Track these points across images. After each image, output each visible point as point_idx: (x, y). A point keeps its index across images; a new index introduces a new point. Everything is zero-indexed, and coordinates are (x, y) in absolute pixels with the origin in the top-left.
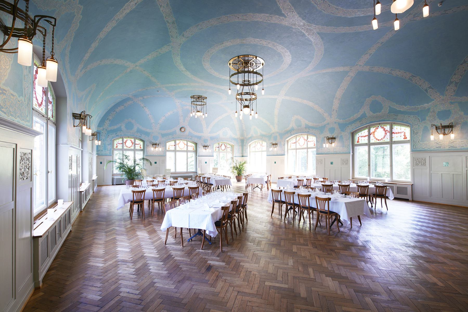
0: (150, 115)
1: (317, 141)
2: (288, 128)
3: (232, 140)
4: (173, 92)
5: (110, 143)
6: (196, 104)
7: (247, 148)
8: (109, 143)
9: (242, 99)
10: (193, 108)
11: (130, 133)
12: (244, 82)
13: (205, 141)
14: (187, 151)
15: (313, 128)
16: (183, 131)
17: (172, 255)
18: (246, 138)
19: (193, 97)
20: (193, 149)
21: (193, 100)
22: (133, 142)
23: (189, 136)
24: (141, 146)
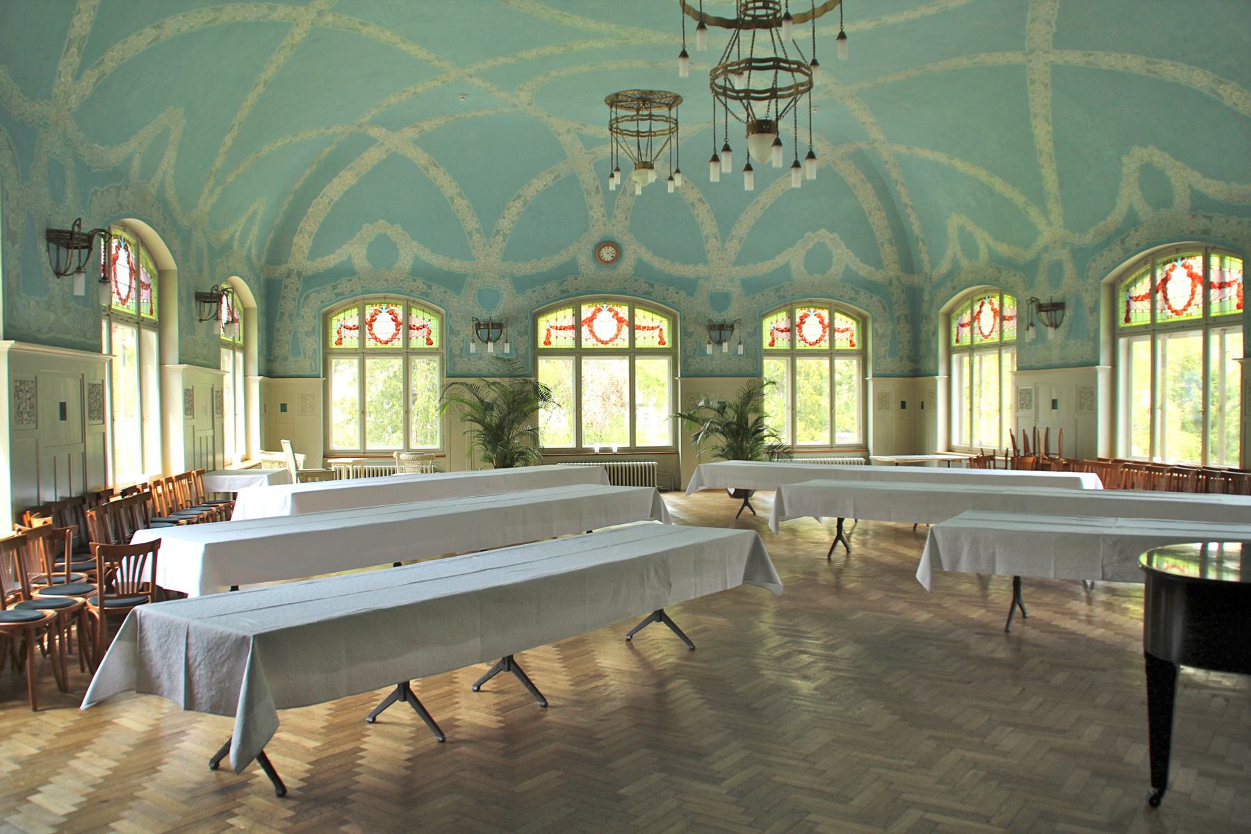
0: (458, 201)
2: (1109, 219)
3: (857, 293)
4: (521, 90)
5: (314, 328)
7: (935, 333)
8: (310, 329)
9: (730, 90)
11: (387, 280)
13: (721, 300)
14: (632, 353)
17: (251, 785)
18: (931, 278)
20: (662, 342)
22: (400, 318)
24: (852, 335)
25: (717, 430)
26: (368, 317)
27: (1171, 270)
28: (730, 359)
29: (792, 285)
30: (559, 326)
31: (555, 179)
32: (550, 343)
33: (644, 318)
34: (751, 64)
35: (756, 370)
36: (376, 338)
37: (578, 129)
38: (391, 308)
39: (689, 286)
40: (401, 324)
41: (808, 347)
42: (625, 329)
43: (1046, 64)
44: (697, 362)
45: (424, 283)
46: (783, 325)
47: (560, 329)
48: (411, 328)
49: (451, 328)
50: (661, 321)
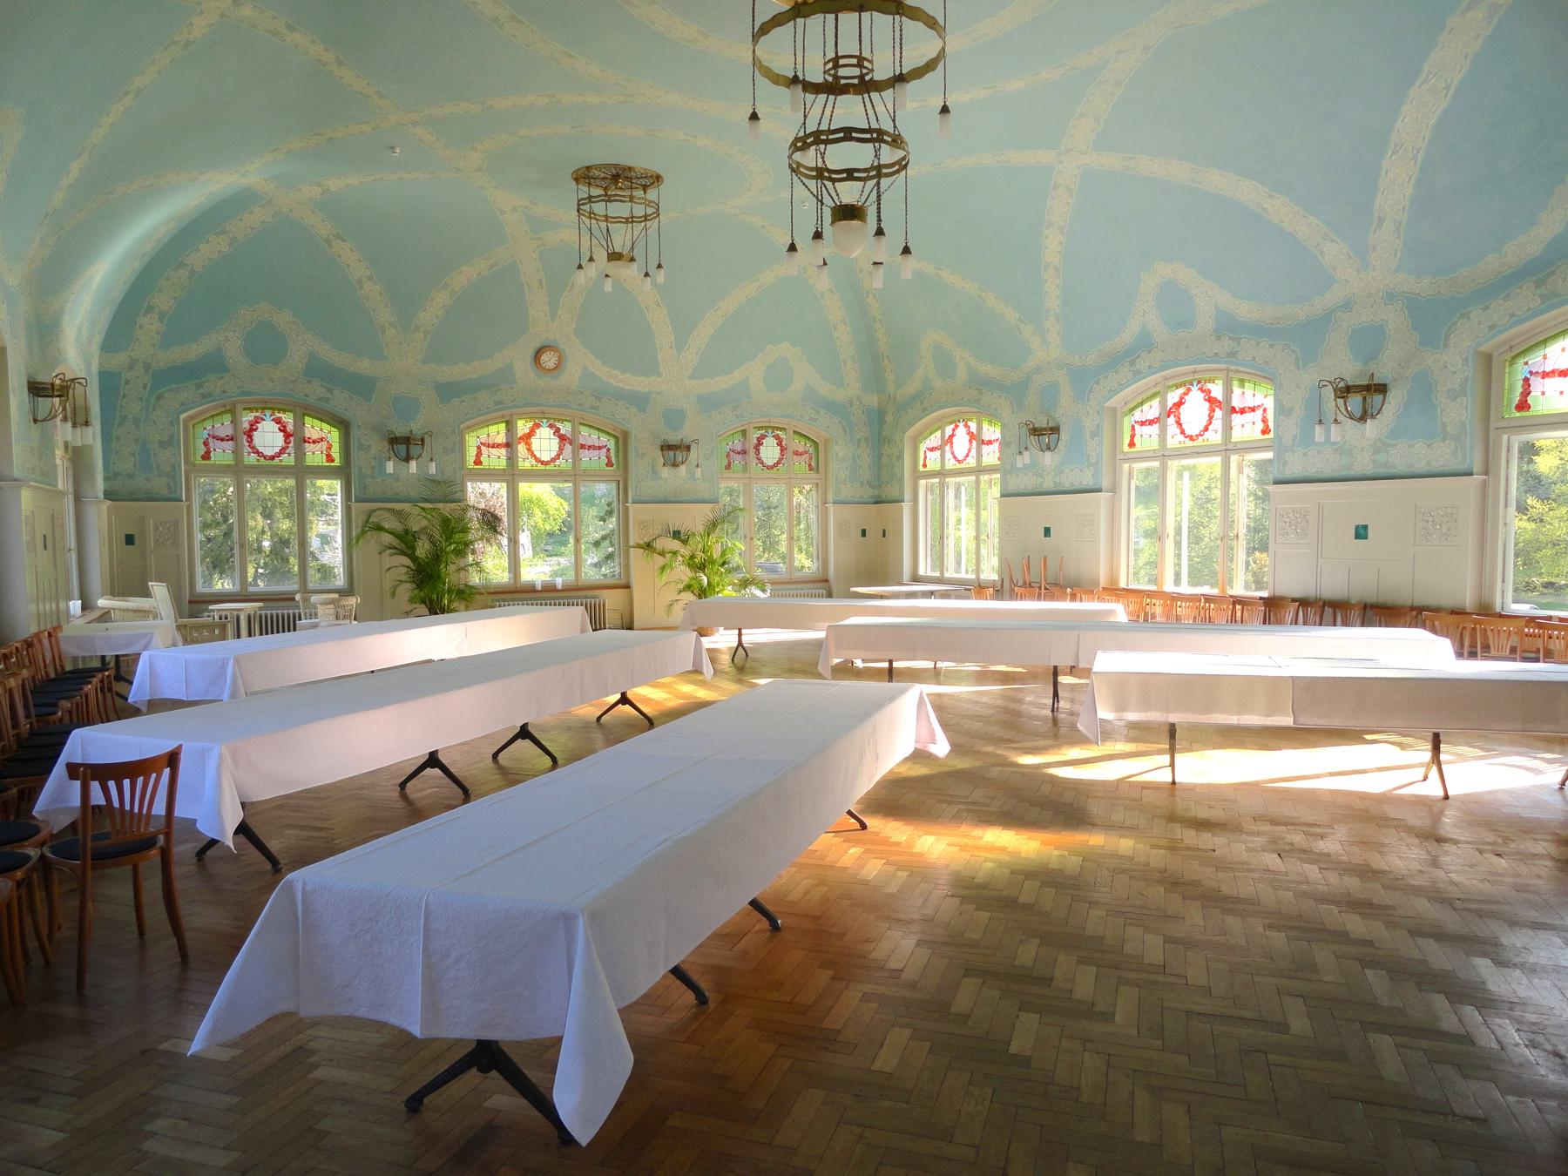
0: (368, 285)
1: (1280, 408)
3: (818, 413)
4: (475, 150)
6: (606, 217)
7: (900, 457)
8: (166, 439)
10: (585, 232)
12: (836, 66)
13: (675, 417)
15: (1261, 331)
16: (551, 365)
17: (314, 1052)
19: (584, 176)
21: (584, 191)
22: (290, 428)
23: (582, 393)
27: (1186, 394)
29: (749, 402)
31: (491, 267)
34: (848, 134)
36: (258, 452)
37: (526, 207)
38: (278, 415)
39: (639, 401)
40: (292, 435)
43: (1078, 167)
45: (322, 386)
48: (305, 442)
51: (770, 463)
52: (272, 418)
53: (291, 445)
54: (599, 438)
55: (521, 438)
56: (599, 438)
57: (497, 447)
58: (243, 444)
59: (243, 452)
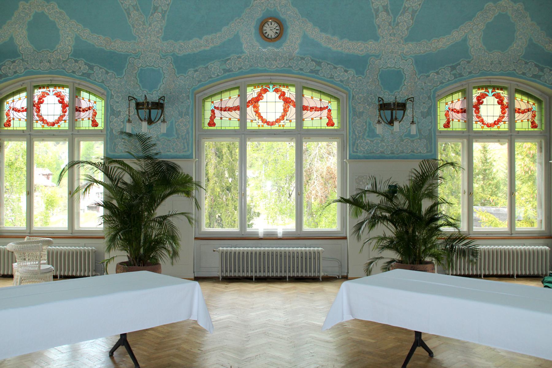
3: (542, 70)
11: (49, 62)
20: (330, 123)
22: (67, 100)
24: (534, 116)
25: (385, 218)
26: (36, 100)
28: (403, 141)
29: (469, 62)
30: (223, 107)
32: (214, 125)
33: (312, 98)
35: (431, 151)
36: (43, 120)
40: (67, 106)
41: (486, 129)
42: (292, 111)
44: (367, 143)
46: (458, 106)
47: (225, 111)
49: (112, 109)
50: (330, 102)
51: (491, 121)
52: (493, 93)
53: (506, 115)
54: (321, 100)
55: (249, 102)
56: (321, 100)
57: (229, 110)
58: (472, 115)
59: (472, 121)
